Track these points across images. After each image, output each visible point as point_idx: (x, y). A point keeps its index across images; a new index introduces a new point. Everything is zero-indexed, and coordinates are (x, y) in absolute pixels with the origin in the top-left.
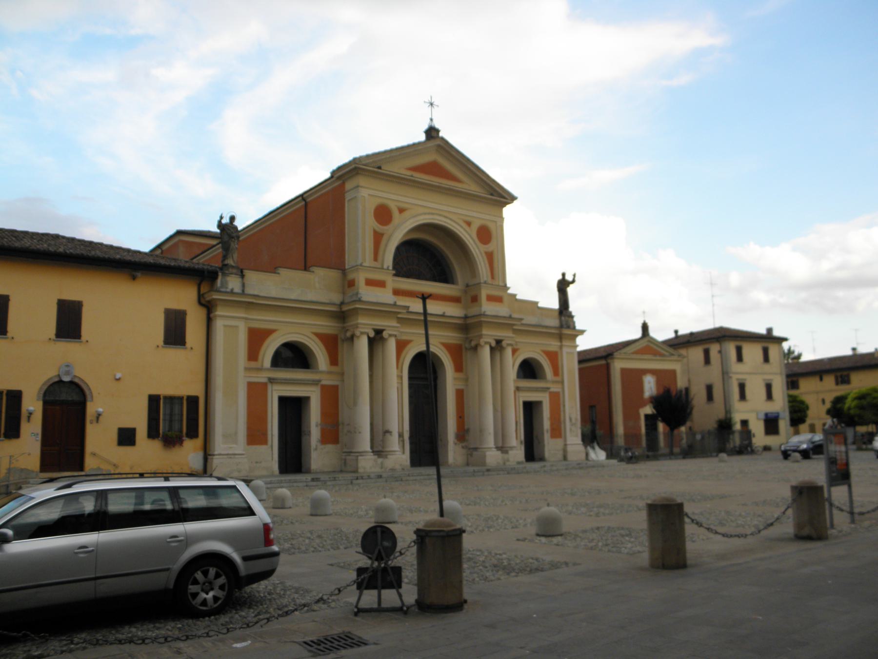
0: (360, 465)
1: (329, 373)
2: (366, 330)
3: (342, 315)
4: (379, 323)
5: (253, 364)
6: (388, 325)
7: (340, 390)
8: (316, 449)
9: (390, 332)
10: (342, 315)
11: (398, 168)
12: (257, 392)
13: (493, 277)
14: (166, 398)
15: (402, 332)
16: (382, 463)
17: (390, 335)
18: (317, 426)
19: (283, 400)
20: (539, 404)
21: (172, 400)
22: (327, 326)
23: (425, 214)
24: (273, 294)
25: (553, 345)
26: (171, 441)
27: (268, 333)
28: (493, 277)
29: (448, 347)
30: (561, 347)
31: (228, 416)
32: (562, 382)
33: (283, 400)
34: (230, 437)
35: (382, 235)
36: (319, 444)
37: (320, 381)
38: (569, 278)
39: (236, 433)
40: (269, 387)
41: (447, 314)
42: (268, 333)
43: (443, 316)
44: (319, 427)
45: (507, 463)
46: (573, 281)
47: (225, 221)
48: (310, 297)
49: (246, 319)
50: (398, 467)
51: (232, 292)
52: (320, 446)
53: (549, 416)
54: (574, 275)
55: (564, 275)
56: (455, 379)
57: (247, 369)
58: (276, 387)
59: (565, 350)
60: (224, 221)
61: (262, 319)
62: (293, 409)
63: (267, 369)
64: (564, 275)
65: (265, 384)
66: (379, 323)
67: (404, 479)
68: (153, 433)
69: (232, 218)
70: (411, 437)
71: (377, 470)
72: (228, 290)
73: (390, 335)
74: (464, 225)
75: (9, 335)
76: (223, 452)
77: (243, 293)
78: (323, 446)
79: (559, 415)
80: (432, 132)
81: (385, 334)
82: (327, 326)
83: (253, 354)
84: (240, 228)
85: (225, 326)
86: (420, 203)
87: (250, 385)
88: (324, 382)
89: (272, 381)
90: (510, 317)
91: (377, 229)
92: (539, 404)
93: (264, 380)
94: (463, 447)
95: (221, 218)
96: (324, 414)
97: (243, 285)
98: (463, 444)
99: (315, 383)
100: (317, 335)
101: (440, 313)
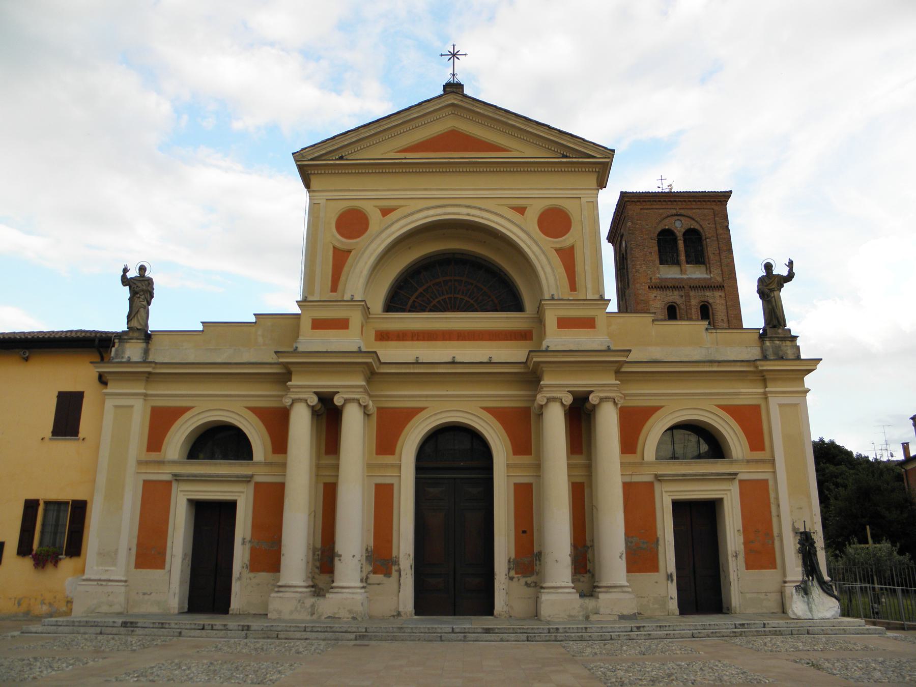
0: (271, 607)
1: (267, 464)
3: (530, 376)
4: (581, 382)
5: (154, 456)
6: (598, 384)
7: (586, 491)
8: (239, 579)
9: (346, 396)
10: (530, 376)
11: (384, 151)
12: (155, 497)
13: (573, 287)
14: (47, 503)
15: (625, 395)
16: (313, 606)
17: (602, 400)
18: (244, 543)
19: (679, 506)
20: (230, 507)
21: (59, 504)
22: (508, 396)
23: (428, 209)
24: (191, 359)
25: (746, 393)
26: (44, 560)
27: (179, 412)
28: (573, 287)
29: (498, 413)
30: (765, 396)
31: (111, 529)
32: (773, 461)
33: (679, 506)
34: (108, 556)
35: (572, 248)
36: (245, 571)
37: (252, 476)
38: (780, 270)
39: (117, 550)
40: (657, 486)
41: (458, 359)
42: (411, 414)
43: (490, 363)
44: (248, 546)
45: (594, 618)
46: (790, 277)
47: (133, 273)
48: (247, 356)
49: (146, 395)
50: (344, 614)
51: (129, 362)
52: (246, 574)
53: (739, 524)
54: (791, 263)
55: (768, 267)
56: (570, 466)
57: (140, 463)
58: (668, 487)
59: (774, 402)
60: (130, 275)
61: (169, 394)
62: (698, 522)
63: (174, 462)
64: (768, 267)
65: (169, 483)
67: (282, 635)
68: (24, 549)
69: (142, 269)
71: (304, 616)
72: (124, 360)
74: (515, 216)
75: (81, 435)
76: (93, 577)
77: (145, 362)
78: (252, 575)
79: (390, 542)
80: (453, 88)
81: (593, 399)
82: (508, 396)
83: (155, 441)
84: (774, 273)
85: (780, 405)
86: (536, 193)
87: (628, 487)
88: (258, 479)
89: (178, 478)
90: (609, 350)
91: (558, 246)
92: (230, 507)
93: (168, 478)
94: (527, 584)
95: (125, 270)
96: (257, 526)
97: (146, 352)
98: (529, 580)
99: (247, 479)
100: (255, 410)
101: (412, 359)
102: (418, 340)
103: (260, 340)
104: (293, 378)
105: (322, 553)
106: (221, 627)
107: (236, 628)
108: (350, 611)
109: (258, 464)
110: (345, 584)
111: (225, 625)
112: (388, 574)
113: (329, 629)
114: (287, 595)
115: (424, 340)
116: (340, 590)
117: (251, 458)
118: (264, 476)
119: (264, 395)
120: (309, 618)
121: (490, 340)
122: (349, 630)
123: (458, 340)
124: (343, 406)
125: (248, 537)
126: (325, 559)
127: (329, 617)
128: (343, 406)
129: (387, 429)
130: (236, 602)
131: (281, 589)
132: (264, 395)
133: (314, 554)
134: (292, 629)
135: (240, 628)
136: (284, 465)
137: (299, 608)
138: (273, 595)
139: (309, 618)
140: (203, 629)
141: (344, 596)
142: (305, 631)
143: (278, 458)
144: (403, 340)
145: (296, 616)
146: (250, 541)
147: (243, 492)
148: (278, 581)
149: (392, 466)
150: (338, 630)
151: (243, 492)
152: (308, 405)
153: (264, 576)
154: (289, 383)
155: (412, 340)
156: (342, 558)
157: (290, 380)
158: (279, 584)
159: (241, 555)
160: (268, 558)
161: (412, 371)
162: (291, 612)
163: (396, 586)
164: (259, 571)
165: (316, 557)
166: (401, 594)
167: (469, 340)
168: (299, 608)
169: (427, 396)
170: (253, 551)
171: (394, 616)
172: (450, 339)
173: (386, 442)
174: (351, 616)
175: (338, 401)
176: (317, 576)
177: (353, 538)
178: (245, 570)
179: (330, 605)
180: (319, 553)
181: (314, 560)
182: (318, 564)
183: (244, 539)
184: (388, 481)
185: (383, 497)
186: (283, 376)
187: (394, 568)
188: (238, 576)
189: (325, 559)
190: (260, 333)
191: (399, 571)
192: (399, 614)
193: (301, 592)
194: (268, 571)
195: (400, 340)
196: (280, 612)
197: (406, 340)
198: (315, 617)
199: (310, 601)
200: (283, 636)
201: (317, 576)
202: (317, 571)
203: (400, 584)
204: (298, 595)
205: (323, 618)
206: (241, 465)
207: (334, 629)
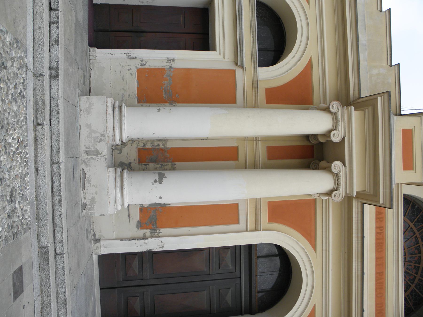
0: (93, 97)
2: (340, 128)
4: (355, 151)
6: (352, 171)
8: (129, 57)
16: (98, 153)
17: (336, 176)
18: (169, 60)
20: (203, 40)
37: (242, 66)
42: (310, 236)
44: (166, 65)
50: (89, 193)
52: (135, 65)
57: (257, 201)
61: (327, 225)
66: (355, 151)
70: (151, 254)
71: (84, 142)
73: (336, 176)
78: (134, 71)
79: (176, 225)
88: (239, 72)
92: (203, 40)
96: (188, 74)
99: (238, 61)
102: (377, 233)
103: (375, 72)
104: (357, 112)
105: (161, 150)
106: (54, 35)
107: (54, 58)
108: (93, 200)
109: (256, 74)
110: (126, 190)
111: (57, 41)
112: (141, 225)
113: (57, 198)
114: (110, 119)
115: (377, 239)
116: (119, 185)
117: (260, 66)
118: (242, 79)
119: (325, 78)
120: (83, 148)
121: (377, 304)
122: (58, 229)
123: (377, 273)
124: (330, 171)
125: (176, 65)
126: (155, 158)
127: (85, 174)
128: (330, 171)
129: (292, 213)
130: (102, 55)
131: (117, 110)
132: (325, 78)
133: (159, 140)
134: (55, 143)
135: (54, 65)
136: (255, 105)
137: (94, 135)
138: (110, 101)
139: (83, 148)
140: (51, 9)
141: (112, 192)
142: (53, 163)
143: (262, 96)
144: (377, 218)
145: (84, 132)
146: (170, 67)
147: (224, 57)
148: (128, 106)
149: (257, 221)
150: (57, 213)
151: (224, 57)
152: (330, 132)
153: (132, 85)
154: (353, 108)
155: (377, 228)
156: (157, 184)
157: (356, 109)
158: (124, 106)
159: (156, 57)
160: (154, 92)
161: (354, 235)
162: (89, 126)
163: (129, 235)
164: (138, 79)
165: (156, 144)
166: (119, 242)
167: (377, 284)
168: (94, 135)
169: (327, 251)
170: (162, 71)
171: (94, 235)
172: (377, 265)
173: (283, 212)
174: (87, 201)
175: (336, 165)
176: (135, 145)
177: (182, 190)
178: (139, 63)
179: (100, 173)
180: (161, 146)
181: (153, 141)
182: (149, 145)
183: (173, 60)
184: (242, 218)
185: (225, 214)
186: (347, 99)
187: (148, 232)
188: (133, 55)
189: (155, 158)
190: (382, 71)
191: (144, 238)
192: (97, 241)
193: (114, 136)
194: (138, 88)
195: (377, 215)
196: (88, 111)
197: (377, 222)
198: (84, 156)
199: (104, 148)
200: (39, 133)
201: (135, 145)
202: (141, 145)
203: (130, 240)
204: (111, 132)
205: (83, 166)
206: (253, 55)
207: (57, 207)
